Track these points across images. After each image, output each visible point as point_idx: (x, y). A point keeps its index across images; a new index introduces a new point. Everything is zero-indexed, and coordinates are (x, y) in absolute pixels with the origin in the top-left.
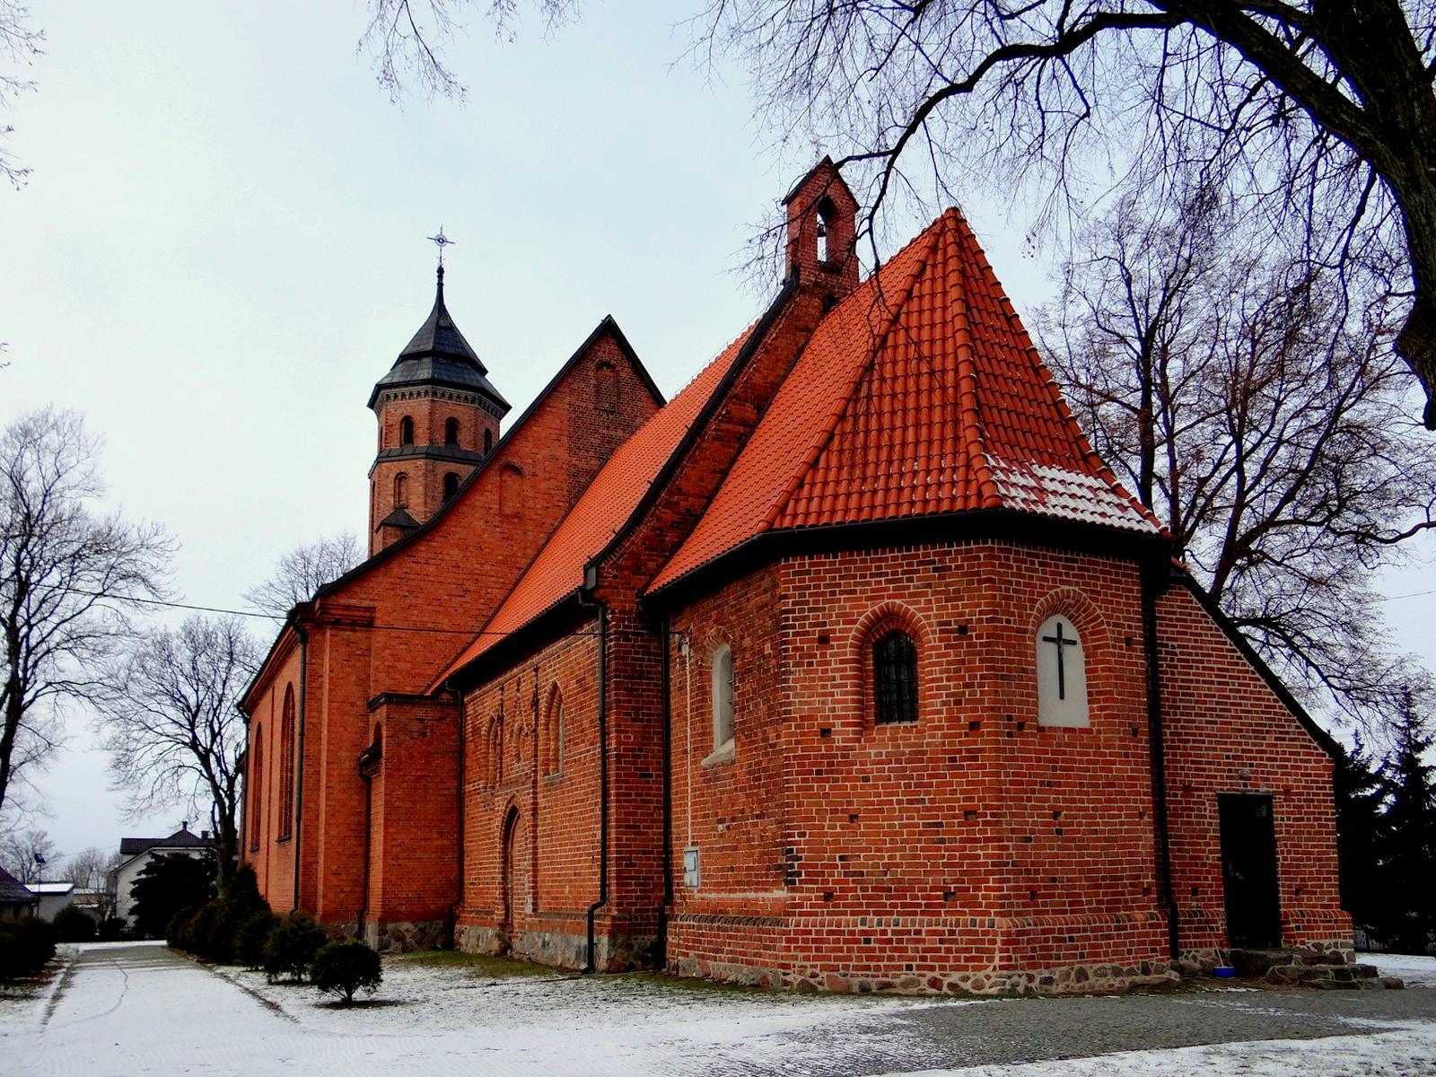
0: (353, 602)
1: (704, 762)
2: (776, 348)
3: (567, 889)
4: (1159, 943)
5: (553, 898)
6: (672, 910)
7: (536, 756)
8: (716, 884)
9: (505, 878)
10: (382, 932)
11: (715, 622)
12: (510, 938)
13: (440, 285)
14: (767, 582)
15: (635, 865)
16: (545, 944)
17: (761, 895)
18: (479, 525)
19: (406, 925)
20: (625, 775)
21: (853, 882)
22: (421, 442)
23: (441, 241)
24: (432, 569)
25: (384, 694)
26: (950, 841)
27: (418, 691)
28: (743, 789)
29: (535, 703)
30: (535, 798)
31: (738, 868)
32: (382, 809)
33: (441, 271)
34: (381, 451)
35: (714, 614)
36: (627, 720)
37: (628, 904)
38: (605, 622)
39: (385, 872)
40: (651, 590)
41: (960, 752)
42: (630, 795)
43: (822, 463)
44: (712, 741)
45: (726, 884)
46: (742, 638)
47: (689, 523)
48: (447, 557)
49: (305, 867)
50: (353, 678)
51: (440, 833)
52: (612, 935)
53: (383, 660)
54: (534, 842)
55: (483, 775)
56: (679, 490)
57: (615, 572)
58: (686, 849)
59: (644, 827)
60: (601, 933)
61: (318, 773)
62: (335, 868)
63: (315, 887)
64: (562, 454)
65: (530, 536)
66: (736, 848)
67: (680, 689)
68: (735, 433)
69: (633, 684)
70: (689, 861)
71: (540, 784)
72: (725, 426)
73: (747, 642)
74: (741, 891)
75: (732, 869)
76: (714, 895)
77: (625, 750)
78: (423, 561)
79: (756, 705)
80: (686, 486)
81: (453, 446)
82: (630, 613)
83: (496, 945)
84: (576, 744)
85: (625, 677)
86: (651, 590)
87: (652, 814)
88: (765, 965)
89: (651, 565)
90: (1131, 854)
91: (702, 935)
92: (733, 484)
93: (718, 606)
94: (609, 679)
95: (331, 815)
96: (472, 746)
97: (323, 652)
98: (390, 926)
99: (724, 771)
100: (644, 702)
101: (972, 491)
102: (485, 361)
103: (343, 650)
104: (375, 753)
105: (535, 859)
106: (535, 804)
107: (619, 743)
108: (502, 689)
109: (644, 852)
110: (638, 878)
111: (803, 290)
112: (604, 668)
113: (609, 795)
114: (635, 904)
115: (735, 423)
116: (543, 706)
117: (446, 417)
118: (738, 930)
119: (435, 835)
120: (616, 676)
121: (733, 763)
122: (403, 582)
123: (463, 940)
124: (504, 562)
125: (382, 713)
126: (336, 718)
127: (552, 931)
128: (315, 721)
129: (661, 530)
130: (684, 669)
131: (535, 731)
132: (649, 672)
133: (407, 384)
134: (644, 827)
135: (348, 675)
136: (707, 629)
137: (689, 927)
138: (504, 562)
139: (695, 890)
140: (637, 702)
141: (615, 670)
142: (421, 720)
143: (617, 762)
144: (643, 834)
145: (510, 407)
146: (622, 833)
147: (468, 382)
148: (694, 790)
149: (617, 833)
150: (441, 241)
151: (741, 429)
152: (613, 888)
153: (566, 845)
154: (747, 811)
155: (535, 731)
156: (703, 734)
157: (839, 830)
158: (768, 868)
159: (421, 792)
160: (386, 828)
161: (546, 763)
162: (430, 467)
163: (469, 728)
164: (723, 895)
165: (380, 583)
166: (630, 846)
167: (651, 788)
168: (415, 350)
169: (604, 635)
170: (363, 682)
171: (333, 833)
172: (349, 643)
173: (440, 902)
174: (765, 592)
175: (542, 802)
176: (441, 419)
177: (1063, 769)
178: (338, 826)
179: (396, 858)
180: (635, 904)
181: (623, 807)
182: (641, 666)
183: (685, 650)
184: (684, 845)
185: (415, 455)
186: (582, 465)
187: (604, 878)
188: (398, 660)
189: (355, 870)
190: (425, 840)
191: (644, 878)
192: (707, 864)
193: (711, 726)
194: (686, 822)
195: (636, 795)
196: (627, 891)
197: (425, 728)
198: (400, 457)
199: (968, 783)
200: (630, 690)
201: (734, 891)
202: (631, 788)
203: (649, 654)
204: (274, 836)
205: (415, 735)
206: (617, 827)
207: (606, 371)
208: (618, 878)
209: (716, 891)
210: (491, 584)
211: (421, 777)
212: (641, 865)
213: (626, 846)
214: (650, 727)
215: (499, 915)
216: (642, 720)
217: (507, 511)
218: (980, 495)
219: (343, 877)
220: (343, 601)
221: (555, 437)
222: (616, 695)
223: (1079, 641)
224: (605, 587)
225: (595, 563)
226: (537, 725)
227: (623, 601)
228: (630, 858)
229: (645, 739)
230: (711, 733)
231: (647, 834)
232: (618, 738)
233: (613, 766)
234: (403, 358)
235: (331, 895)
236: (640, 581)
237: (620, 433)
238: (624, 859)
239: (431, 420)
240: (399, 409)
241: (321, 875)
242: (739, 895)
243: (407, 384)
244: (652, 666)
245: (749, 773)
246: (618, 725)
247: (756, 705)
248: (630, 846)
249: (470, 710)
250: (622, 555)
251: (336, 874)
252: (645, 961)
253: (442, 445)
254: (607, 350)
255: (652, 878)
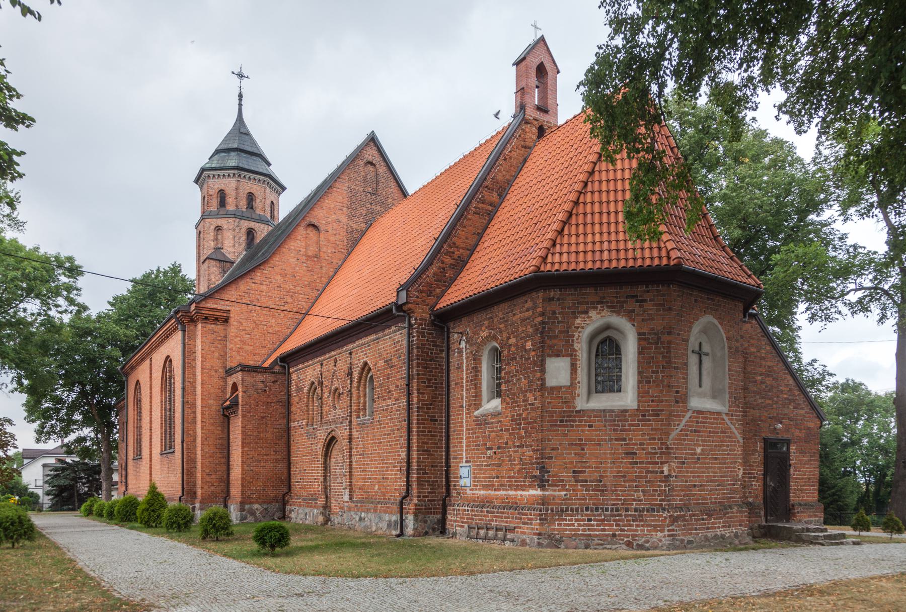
0: (216, 306)
1: (476, 413)
2: (510, 158)
3: (377, 487)
4: (743, 521)
5: (365, 492)
6: (450, 501)
7: (351, 406)
8: (483, 486)
9: (325, 479)
10: (242, 510)
11: (486, 328)
12: (329, 515)
13: (240, 105)
14: (529, 304)
15: (427, 474)
16: (361, 519)
17: (519, 493)
18: (293, 261)
19: (256, 506)
20: (422, 420)
21: (581, 486)
22: (231, 207)
23: (241, 76)
24: (264, 287)
25: (240, 365)
26: (640, 463)
27: (257, 364)
28: (508, 430)
29: (350, 374)
30: (350, 432)
31: (502, 477)
32: (240, 437)
33: (240, 96)
34: (203, 212)
35: (486, 323)
36: (423, 386)
37: (423, 497)
38: (410, 325)
39: (243, 474)
40: (438, 307)
41: (648, 411)
42: (425, 432)
43: (566, 232)
44: (481, 400)
45: (493, 486)
46: (509, 338)
47: (460, 264)
48: (274, 281)
49: (188, 470)
50: (216, 354)
51: (276, 452)
52: (416, 515)
53: (236, 344)
54: (350, 459)
55: (305, 417)
56: (454, 244)
57: (417, 294)
58: (461, 465)
59: (433, 451)
60: (408, 513)
61: (194, 412)
62: (208, 471)
63: (195, 482)
64: (344, 219)
65: (324, 270)
66: (501, 465)
67: (458, 368)
68: (486, 210)
69: (427, 364)
70: (464, 471)
71: (354, 423)
72: (481, 205)
73: (512, 341)
74: (503, 490)
75: (497, 477)
76: (482, 492)
77: (422, 404)
78: (259, 282)
79: (518, 380)
80: (459, 243)
81: (251, 210)
82: (425, 320)
83: (321, 519)
84: (384, 400)
85: (422, 360)
86: (438, 307)
87: (437, 444)
88: (524, 533)
89: (438, 291)
90: (731, 472)
91: (475, 515)
92: (487, 242)
93: (490, 318)
94: (413, 360)
95: (204, 439)
96: (296, 399)
97: (195, 336)
98: (247, 507)
99: (492, 418)
100: (433, 376)
101: (664, 253)
102: (270, 159)
103: (209, 336)
104: (235, 404)
105: (351, 468)
106: (350, 435)
107: (419, 400)
108: (322, 364)
109: (432, 466)
110: (429, 481)
111: (527, 122)
112: (410, 352)
113: (412, 432)
114: (427, 497)
115: (487, 204)
116: (356, 375)
117: (247, 192)
118: (503, 513)
119: (272, 453)
120: (418, 359)
121: (499, 414)
122: (247, 295)
123: (293, 515)
124: (309, 285)
125: (238, 377)
126: (206, 379)
127: (368, 511)
128: (192, 380)
129: (444, 269)
130: (462, 356)
131: (350, 391)
132: (437, 357)
133: (221, 169)
134: (433, 451)
135: (213, 352)
136: (481, 332)
137: (465, 510)
138: (309, 285)
139: (468, 489)
140: (429, 375)
141: (417, 355)
142: (263, 382)
143: (418, 412)
144: (432, 455)
145: (284, 189)
146: (420, 454)
147: (261, 171)
148: (468, 430)
149: (418, 454)
150: (241, 76)
151: (490, 208)
152: (414, 487)
153: (376, 460)
154: (510, 443)
155: (350, 391)
156: (476, 396)
157: (573, 455)
158: (525, 477)
159: (264, 426)
160: (243, 447)
161: (358, 410)
162: (237, 224)
163: (294, 388)
164: (490, 492)
165: (232, 294)
166: (425, 462)
167: (437, 428)
168: (226, 147)
169: (410, 335)
170: (223, 357)
171: (206, 450)
172: (213, 332)
173: (276, 492)
174: (528, 310)
175: (355, 434)
176: (243, 193)
177: (701, 422)
178: (209, 445)
179: (249, 466)
180: (427, 497)
181: (421, 439)
182: (432, 353)
183: (463, 345)
184: (460, 462)
185: (228, 215)
186: (355, 226)
187: (408, 481)
188: (245, 344)
189: (220, 472)
190: (267, 455)
191: (432, 481)
192: (477, 474)
193: (481, 391)
194: (462, 447)
195: (428, 432)
196: (423, 489)
197: (266, 387)
198: (217, 215)
199: (652, 430)
200: (426, 368)
201: (499, 490)
202: (425, 428)
203: (437, 346)
204: (157, 449)
205: (260, 391)
206: (418, 451)
207: (371, 168)
208: (418, 481)
209: (483, 490)
210: (300, 299)
211: (264, 417)
212: (431, 474)
213: (423, 462)
214: (437, 391)
215: (321, 501)
216: (432, 387)
217: (310, 253)
218: (669, 258)
219: (213, 477)
220: (209, 305)
221: (339, 207)
222: (417, 370)
223: (690, 352)
224: (411, 303)
225: (406, 287)
226: (351, 387)
227: (421, 313)
228: (424, 470)
229: (434, 398)
230: (481, 396)
231: (434, 455)
232: (418, 397)
233: (415, 414)
234: (217, 152)
235: (206, 487)
236: (432, 300)
237: (378, 208)
238: (421, 469)
239: (237, 193)
240: (216, 184)
241: (199, 475)
242: (502, 493)
243: (221, 169)
244: (438, 354)
245: (512, 421)
246: (418, 389)
247: (518, 380)
248: (425, 462)
249: (294, 377)
250: (421, 283)
251: (209, 475)
252: (434, 529)
253: (244, 210)
254: (371, 154)
255: (437, 481)
